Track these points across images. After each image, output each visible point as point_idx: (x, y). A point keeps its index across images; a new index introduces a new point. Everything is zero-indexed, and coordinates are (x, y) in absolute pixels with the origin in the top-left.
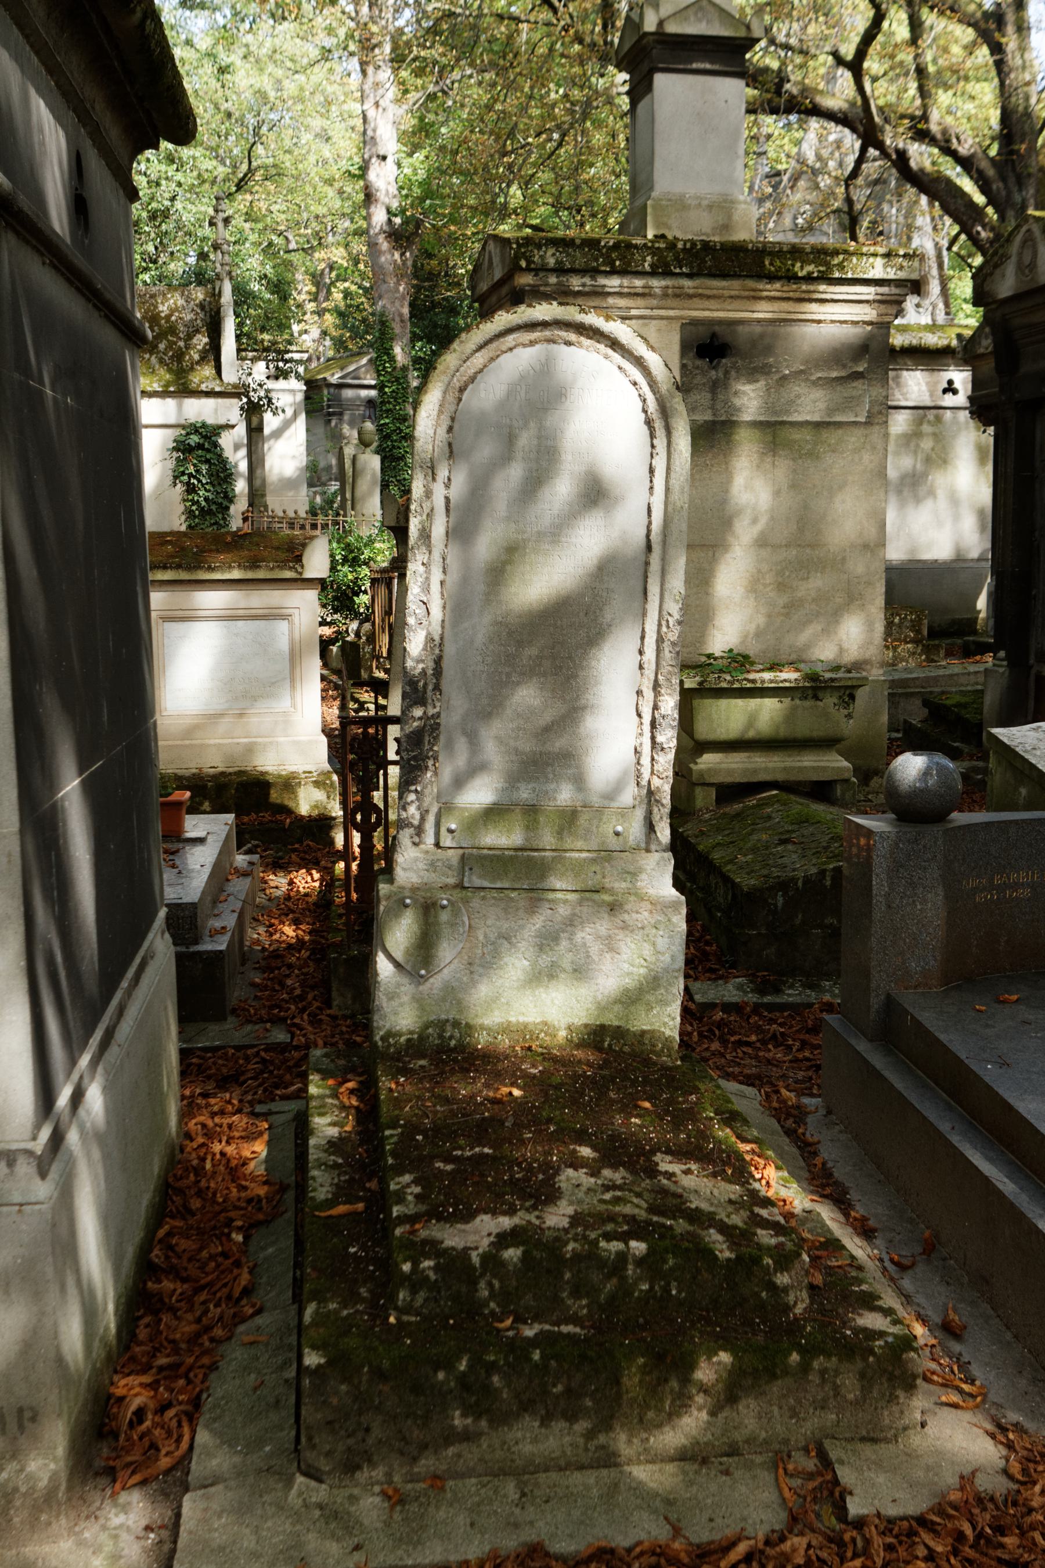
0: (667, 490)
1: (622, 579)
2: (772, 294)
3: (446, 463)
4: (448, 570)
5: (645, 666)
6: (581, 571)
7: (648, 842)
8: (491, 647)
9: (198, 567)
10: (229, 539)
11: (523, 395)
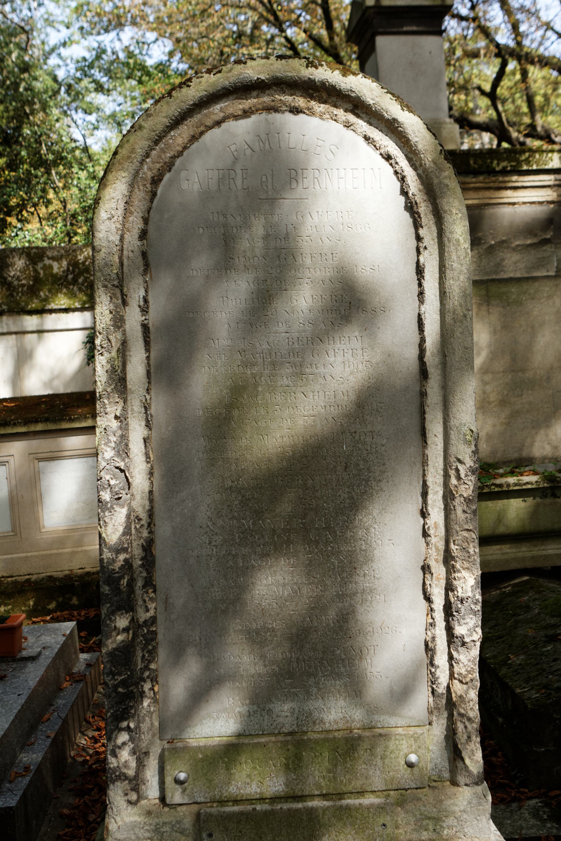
0: (443, 294)
1: (392, 416)
2: (477, 185)
3: (140, 280)
4: (154, 423)
5: (431, 532)
6: (334, 411)
7: (453, 771)
8: (220, 522)
9: (62, 420)
10: (88, 397)
11: (239, 182)
